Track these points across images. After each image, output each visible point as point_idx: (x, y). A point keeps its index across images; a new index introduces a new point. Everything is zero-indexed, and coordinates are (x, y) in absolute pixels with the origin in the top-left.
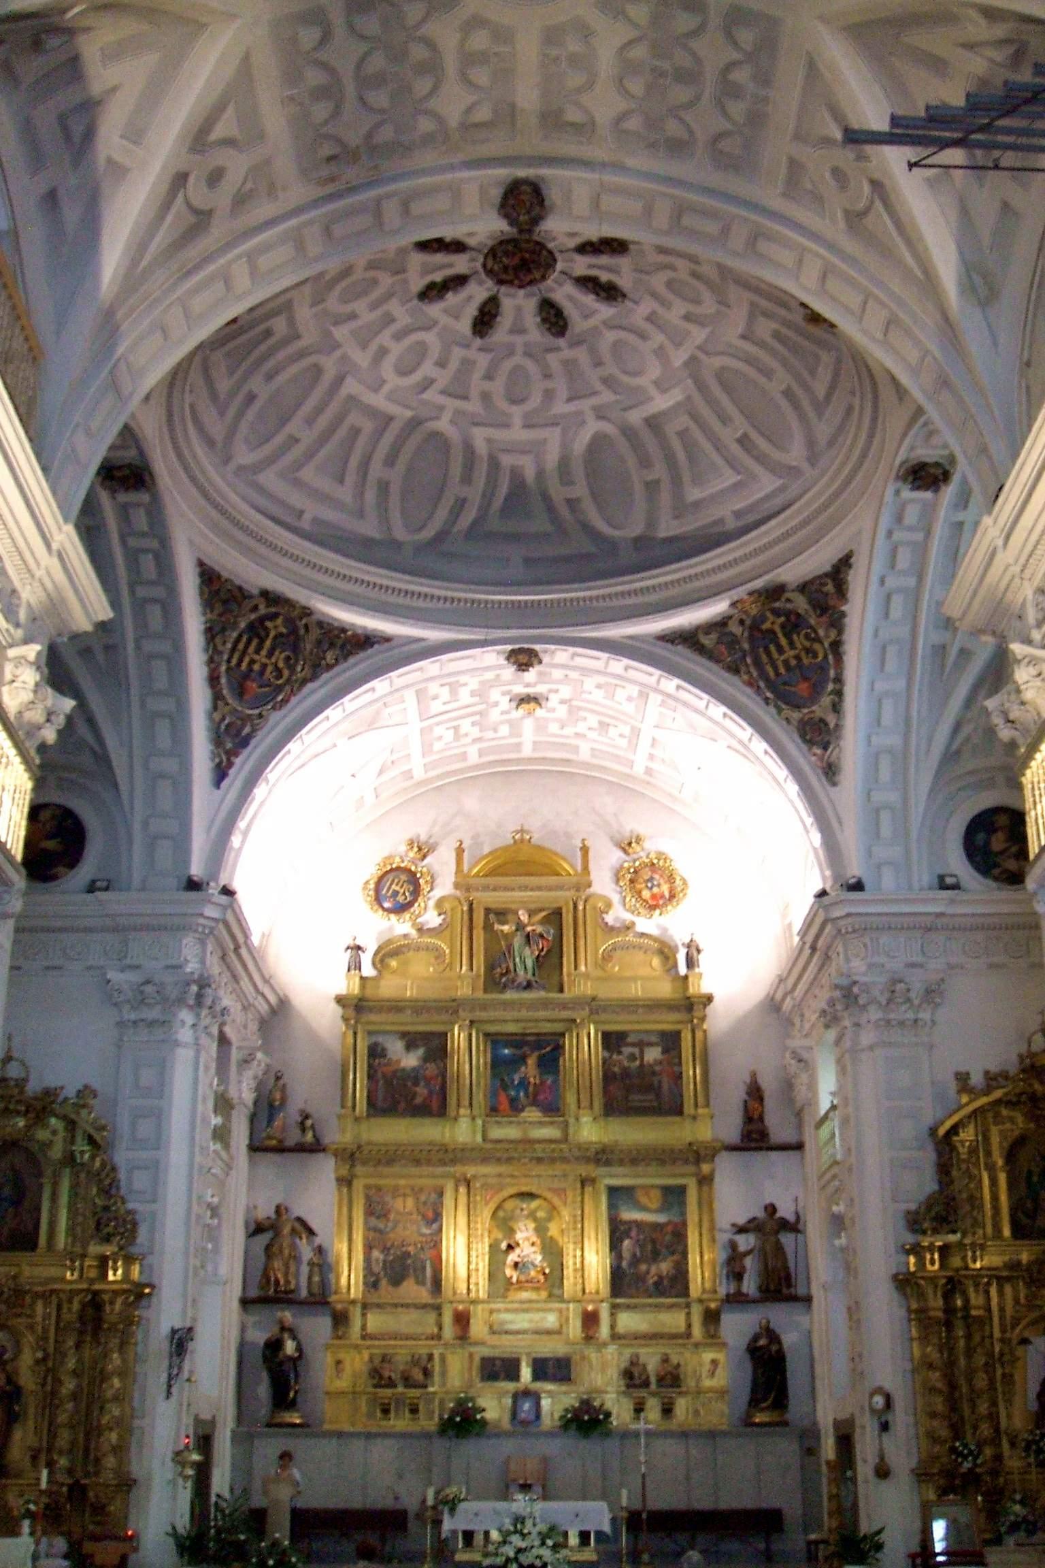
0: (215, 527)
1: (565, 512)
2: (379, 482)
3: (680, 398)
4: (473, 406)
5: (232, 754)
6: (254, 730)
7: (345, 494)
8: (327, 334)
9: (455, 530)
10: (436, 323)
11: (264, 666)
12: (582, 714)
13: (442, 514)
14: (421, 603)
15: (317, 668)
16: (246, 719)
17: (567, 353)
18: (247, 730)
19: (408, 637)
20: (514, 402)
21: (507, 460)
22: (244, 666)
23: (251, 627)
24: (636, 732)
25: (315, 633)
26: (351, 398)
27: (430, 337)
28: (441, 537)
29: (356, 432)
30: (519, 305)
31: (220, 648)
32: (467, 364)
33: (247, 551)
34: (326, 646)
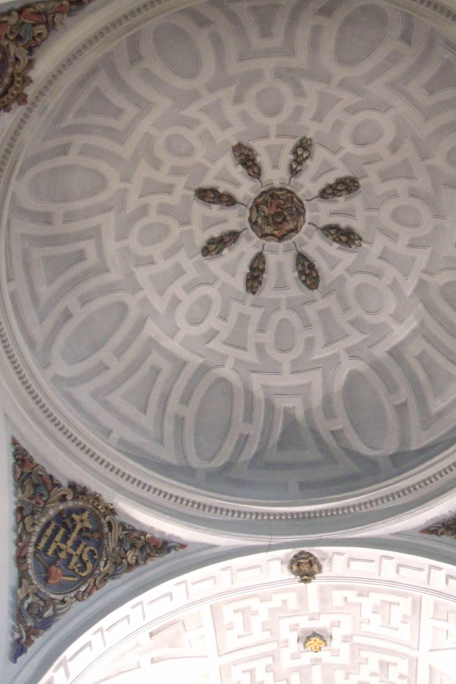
0: (31, 413)
2: (177, 416)
3: (415, 324)
4: (250, 356)
5: (32, 633)
6: (55, 615)
7: (147, 421)
8: (131, 275)
9: (240, 460)
10: (217, 279)
11: (70, 556)
12: (364, 654)
13: (228, 448)
14: (211, 516)
15: (120, 566)
16: (47, 602)
17: (322, 304)
18: (48, 613)
19: (202, 544)
20: (283, 351)
21: (281, 403)
22: (50, 552)
23: (60, 517)
24: (414, 663)
25: (118, 533)
26: (151, 340)
27: (212, 291)
28: (228, 466)
29: (156, 371)
30: (280, 258)
31: (29, 529)
32: (243, 318)
34: (127, 547)
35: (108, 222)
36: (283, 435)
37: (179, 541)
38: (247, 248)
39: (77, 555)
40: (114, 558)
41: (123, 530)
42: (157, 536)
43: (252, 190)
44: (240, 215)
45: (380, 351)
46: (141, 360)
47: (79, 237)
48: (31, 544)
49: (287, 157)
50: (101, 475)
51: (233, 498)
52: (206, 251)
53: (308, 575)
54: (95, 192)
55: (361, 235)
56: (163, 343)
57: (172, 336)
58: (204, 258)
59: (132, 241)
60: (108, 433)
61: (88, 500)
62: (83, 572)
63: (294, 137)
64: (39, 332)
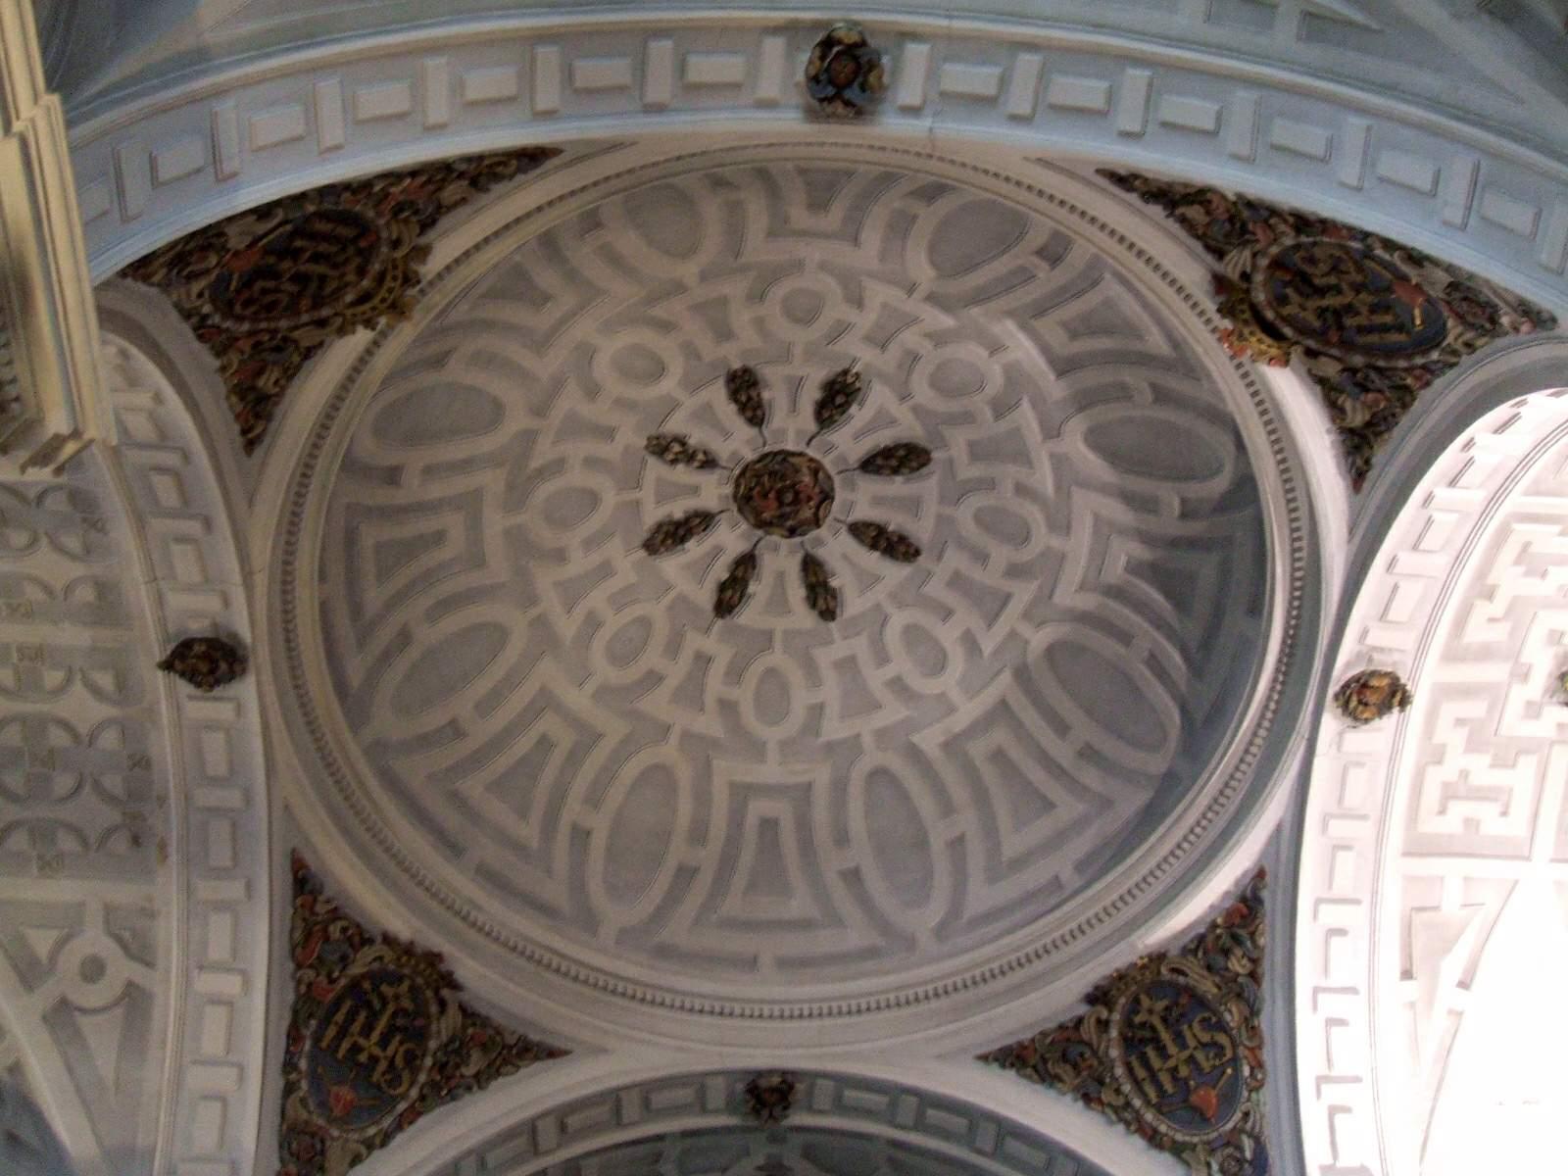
1: (1195, 528)
3: (1010, 325)
4: (1023, 593)
6: (1257, 1140)
7: (1069, 807)
8: (830, 747)
9: (1183, 688)
10: (878, 607)
15: (1246, 990)
16: (1231, 1141)
18: (1248, 1144)
20: (1027, 539)
23: (1129, 1043)
27: (898, 620)
29: (999, 756)
32: (957, 581)
33: (1018, 990)
35: (727, 770)
36: (1168, 595)
37: (1250, 876)
38: (836, 547)
39: (1195, 1048)
40: (1229, 993)
41: (1196, 955)
42: (1228, 904)
43: (734, 526)
44: (776, 548)
45: (1056, 389)
46: (970, 771)
47: (736, 821)
48: (1142, 1112)
49: (682, 474)
50: (1090, 948)
51: (1221, 750)
52: (828, 615)
53: (1393, 694)
54: (671, 787)
55: (839, 369)
56: (957, 729)
57: (952, 709)
58: (838, 619)
59: (772, 735)
60: (1056, 883)
61: (1119, 989)
62: (1225, 1055)
63: (644, 462)
64: (856, 936)
